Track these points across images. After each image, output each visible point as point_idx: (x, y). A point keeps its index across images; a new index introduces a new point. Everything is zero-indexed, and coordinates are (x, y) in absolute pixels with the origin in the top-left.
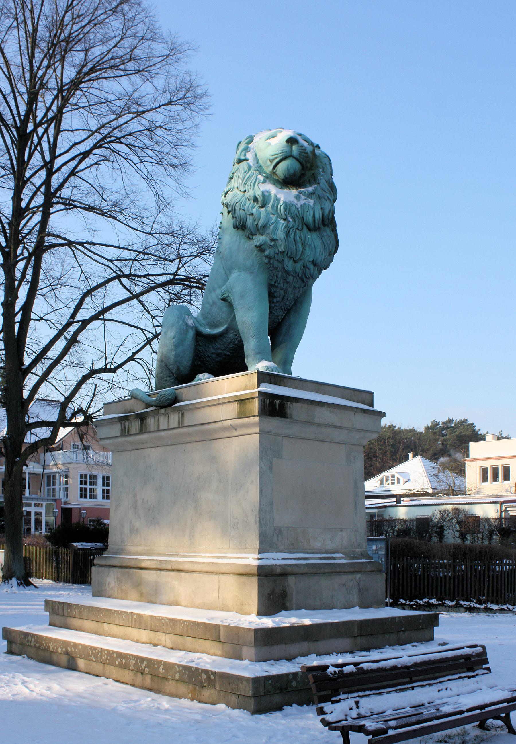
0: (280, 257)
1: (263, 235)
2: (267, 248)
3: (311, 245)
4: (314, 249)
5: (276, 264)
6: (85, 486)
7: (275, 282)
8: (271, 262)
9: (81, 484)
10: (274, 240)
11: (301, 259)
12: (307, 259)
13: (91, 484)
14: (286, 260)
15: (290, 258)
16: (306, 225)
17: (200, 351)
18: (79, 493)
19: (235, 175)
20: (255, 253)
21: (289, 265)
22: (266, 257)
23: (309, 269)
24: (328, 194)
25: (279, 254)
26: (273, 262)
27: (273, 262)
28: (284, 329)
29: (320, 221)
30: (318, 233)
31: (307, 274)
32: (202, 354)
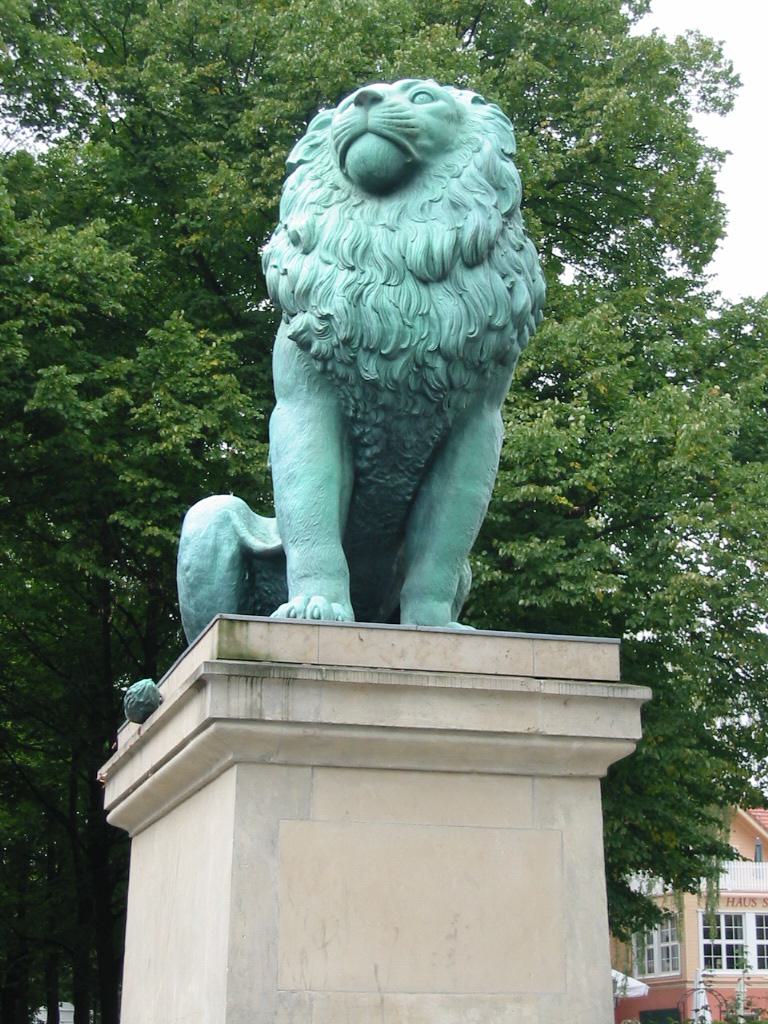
1: (305, 312)
2: (314, 338)
3: (428, 313)
4: (437, 324)
5: (341, 370)
6: (717, 942)
8: (329, 367)
9: (707, 935)
10: (326, 318)
11: (403, 351)
13: (729, 935)
15: (371, 351)
16: (411, 271)
17: (266, 592)
18: (702, 957)
20: (297, 354)
21: (370, 369)
22: (315, 357)
23: (433, 369)
24: (477, 196)
26: (334, 367)
27: (334, 367)
28: (421, 513)
29: (423, 265)
30: (447, 285)
32: (272, 598)
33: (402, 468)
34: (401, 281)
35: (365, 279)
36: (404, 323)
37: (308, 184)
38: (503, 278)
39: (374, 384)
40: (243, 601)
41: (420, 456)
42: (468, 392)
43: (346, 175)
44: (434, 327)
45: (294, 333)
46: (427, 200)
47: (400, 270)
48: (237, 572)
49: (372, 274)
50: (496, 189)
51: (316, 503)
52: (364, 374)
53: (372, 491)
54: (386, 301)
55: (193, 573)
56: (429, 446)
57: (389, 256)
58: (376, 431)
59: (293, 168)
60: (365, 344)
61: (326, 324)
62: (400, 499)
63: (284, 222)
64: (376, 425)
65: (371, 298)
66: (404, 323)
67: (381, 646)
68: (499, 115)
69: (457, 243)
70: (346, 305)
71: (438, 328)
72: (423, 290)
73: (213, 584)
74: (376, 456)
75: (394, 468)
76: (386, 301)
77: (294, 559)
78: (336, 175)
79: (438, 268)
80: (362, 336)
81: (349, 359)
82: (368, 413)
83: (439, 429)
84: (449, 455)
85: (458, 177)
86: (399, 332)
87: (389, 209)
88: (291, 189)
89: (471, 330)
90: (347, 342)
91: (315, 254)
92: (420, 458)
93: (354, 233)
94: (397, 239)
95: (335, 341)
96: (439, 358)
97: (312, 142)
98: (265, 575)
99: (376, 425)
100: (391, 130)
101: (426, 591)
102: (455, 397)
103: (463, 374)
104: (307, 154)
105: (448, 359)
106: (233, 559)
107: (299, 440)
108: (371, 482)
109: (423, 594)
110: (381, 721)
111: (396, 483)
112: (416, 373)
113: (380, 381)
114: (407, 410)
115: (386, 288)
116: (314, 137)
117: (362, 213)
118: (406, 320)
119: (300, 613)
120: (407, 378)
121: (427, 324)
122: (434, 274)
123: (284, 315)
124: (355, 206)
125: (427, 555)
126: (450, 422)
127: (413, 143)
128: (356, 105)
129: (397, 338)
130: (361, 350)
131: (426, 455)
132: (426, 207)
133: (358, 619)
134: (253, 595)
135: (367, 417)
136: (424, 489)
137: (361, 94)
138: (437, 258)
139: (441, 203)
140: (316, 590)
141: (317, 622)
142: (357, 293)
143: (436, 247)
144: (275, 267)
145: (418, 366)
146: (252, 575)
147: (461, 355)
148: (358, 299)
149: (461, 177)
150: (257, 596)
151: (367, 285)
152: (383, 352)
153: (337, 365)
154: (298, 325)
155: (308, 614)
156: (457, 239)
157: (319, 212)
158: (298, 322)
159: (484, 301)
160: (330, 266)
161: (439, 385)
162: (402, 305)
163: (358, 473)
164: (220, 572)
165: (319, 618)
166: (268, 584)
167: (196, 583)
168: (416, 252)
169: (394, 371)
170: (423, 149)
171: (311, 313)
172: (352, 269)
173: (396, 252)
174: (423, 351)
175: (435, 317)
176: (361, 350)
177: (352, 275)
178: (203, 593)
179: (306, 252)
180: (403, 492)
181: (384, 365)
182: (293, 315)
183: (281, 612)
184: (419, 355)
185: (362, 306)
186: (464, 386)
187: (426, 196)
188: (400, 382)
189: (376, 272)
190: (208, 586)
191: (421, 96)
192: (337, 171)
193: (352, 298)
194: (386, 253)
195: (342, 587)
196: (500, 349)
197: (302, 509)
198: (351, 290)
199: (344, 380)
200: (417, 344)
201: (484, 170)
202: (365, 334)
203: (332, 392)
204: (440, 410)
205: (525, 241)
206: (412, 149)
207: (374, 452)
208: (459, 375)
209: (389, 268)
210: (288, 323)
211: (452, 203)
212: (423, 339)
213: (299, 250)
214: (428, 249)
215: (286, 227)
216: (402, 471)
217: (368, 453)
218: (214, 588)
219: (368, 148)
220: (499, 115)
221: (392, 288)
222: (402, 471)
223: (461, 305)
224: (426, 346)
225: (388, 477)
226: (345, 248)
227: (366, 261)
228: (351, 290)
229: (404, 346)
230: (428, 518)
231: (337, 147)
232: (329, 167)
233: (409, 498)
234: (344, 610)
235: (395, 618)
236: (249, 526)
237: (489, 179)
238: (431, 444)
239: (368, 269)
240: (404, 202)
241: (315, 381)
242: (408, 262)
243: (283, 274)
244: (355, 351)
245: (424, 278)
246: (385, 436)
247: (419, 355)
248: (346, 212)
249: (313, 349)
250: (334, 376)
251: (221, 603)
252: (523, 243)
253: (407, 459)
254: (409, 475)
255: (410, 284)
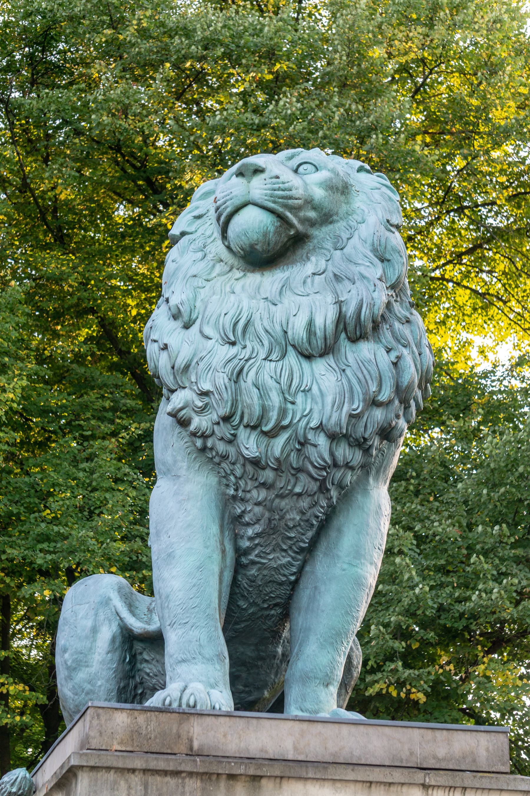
0: (224, 430)
2: (193, 415)
3: (310, 389)
4: (319, 400)
5: (221, 447)
7: (236, 490)
11: (285, 428)
12: (303, 423)
14: (243, 434)
16: (294, 346)
17: (148, 675)
19: (186, 237)
21: (250, 445)
23: (315, 446)
25: (221, 423)
28: (304, 595)
29: (305, 340)
30: (330, 359)
31: (313, 459)
33: (285, 547)
34: (284, 355)
35: (246, 354)
36: (285, 399)
37: (191, 256)
38: (388, 352)
39: (256, 463)
40: (122, 685)
41: (303, 534)
42: (352, 468)
43: (229, 248)
44: (317, 403)
45: (173, 409)
46: (309, 273)
47: (284, 344)
48: (117, 654)
49: (253, 349)
50: (382, 261)
51: (194, 586)
52: (245, 452)
53: (253, 571)
54: (267, 377)
55: (72, 655)
56: (312, 525)
57: (270, 331)
58: (258, 510)
59: (175, 241)
60: (245, 420)
61: (206, 400)
62: (284, 579)
63: (166, 296)
64: (258, 504)
65: (252, 374)
66: (285, 399)
67: (264, 736)
68: (387, 186)
69: (341, 319)
70: (227, 380)
71: (320, 405)
72: (305, 364)
73: (92, 666)
74: (258, 535)
75: (277, 548)
76: (267, 377)
77: (173, 640)
78: (218, 247)
79: (320, 343)
80: (243, 414)
81: (229, 436)
82: (249, 492)
83: (322, 507)
84: (333, 534)
85: (342, 249)
86: (280, 407)
87: (270, 281)
88: (173, 261)
89: (355, 406)
90: (226, 419)
91: (195, 329)
92: (304, 537)
93: (236, 306)
94: (279, 313)
95: (215, 417)
96: (322, 435)
97: (196, 213)
98: (146, 657)
99: (258, 504)
100: (274, 202)
101: (311, 675)
102: (338, 475)
103: (347, 451)
104: (189, 225)
105: (333, 437)
106: (113, 640)
107: (183, 515)
108: (253, 563)
109: (306, 679)
110: (349, 612)
111: (279, 562)
112: (299, 450)
113: (261, 458)
114: (289, 488)
115: (267, 363)
116: (197, 208)
117: (243, 287)
118: (287, 396)
119: (175, 700)
120: (288, 455)
121: (309, 401)
122: (317, 348)
123: (165, 391)
124: (237, 279)
125: (311, 637)
126: (335, 500)
127: (296, 216)
128: (237, 176)
129: (279, 415)
130: (242, 427)
131: (310, 534)
132: (309, 280)
133: (236, 709)
134: (133, 677)
135: (248, 496)
136: (307, 568)
137: (243, 165)
138: (319, 334)
139: (323, 276)
140: (197, 675)
141: (193, 711)
142: (237, 369)
143: (319, 322)
144: (155, 341)
145: (300, 443)
146: (133, 657)
147: (345, 431)
148: (238, 376)
149: (345, 250)
150: (138, 679)
151: (247, 361)
152: (265, 429)
153: (217, 442)
154: (178, 401)
155: (184, 701)
156: (340, 312)
157: (200, 285)
158: (178, 399)
159: (368, 377)
160: (210, 341)
161: (322, 463)
162: (284, 380)
163: (240, 553)
164: (99, 654)
165: (195, 706)
166: (150, 666)
167: (74, 665)
168: (298, 329)
169: (275, 448)
170: (304, 221)
171: (191, 389)
172: (233, 344)
173: (278, 328)
174: (305, 429)
175: (318, 393)
176: (242, 427)
177: (234, 350)
178: (81, 675)
179: (187, 326)
180: (286, 572)
181: (264, 440)
182: (173, 391)
183: (155, 700)
184: (301, 432)
185: (242, 382)
186: (348, 463)
187: (309, 268)
188: (282, 459)
189: (257, 347)
190: (87, 669)
191: (305, 166)
192: (219, 242)
193: (232, 374)
194: (268, 328)
195: (221, 671)
196: (124, 632)
197: (180, 590)
198: (231, 366)
199: (225, 457)
200: (299, 421)
201: (369, 241)
202: (246, 411)
203: (212, 469)
204: (323, 489)
205: (411, 314)
206: (295, 221)
207: (256, 531)
208: (344, 452)
209: (271, 344)
210: (168, 399)
211: (335, 275)
212: (306, 416)
213: (179, 324)
214: (310, 324)
215: (167, 301)
216: (285, 551)
217: (250, 532)
218: (93, 670)
219: (252, 223)
220: (387, 186)
221: (273, 364)
222: (285, 551)
223: (344, 381)
224: (308, 423)
225: (271, 557)
226: (228, 322)
227: (247, 336)
228: (231, 366)
229: (285, 422)
230: (313, 599)
231: (218, 219)
232: (212, 239)
233: (293, 578)
234: (223, 698)
235: (278, 706)
236: (131, 607)
237: (375, 251)
238: (315, 523)
239: (248, 343)
240: (287, 274)
241: (195, 458)
242: (290, 338)
243: (163, 349)
244: (236, 428)
245: (306, 353)
246: (267, 515)
247: (301, 432)
248: (228, 286)
249: (192, 427)
250: (214, 453)
251: (100, 686)
252: (408, 315)
253: (290, 538)
254: (293, 555)
255: (292, 357)
